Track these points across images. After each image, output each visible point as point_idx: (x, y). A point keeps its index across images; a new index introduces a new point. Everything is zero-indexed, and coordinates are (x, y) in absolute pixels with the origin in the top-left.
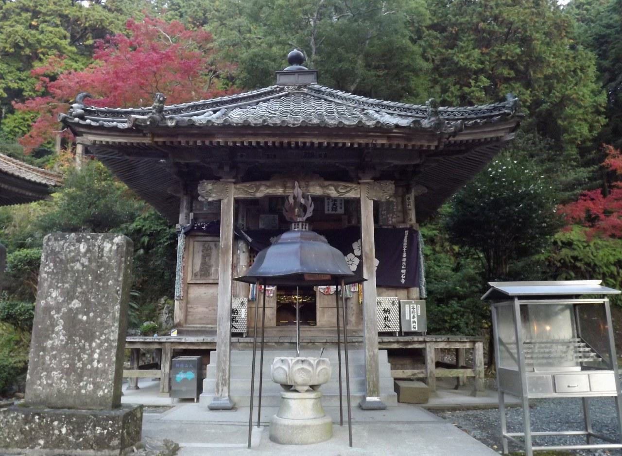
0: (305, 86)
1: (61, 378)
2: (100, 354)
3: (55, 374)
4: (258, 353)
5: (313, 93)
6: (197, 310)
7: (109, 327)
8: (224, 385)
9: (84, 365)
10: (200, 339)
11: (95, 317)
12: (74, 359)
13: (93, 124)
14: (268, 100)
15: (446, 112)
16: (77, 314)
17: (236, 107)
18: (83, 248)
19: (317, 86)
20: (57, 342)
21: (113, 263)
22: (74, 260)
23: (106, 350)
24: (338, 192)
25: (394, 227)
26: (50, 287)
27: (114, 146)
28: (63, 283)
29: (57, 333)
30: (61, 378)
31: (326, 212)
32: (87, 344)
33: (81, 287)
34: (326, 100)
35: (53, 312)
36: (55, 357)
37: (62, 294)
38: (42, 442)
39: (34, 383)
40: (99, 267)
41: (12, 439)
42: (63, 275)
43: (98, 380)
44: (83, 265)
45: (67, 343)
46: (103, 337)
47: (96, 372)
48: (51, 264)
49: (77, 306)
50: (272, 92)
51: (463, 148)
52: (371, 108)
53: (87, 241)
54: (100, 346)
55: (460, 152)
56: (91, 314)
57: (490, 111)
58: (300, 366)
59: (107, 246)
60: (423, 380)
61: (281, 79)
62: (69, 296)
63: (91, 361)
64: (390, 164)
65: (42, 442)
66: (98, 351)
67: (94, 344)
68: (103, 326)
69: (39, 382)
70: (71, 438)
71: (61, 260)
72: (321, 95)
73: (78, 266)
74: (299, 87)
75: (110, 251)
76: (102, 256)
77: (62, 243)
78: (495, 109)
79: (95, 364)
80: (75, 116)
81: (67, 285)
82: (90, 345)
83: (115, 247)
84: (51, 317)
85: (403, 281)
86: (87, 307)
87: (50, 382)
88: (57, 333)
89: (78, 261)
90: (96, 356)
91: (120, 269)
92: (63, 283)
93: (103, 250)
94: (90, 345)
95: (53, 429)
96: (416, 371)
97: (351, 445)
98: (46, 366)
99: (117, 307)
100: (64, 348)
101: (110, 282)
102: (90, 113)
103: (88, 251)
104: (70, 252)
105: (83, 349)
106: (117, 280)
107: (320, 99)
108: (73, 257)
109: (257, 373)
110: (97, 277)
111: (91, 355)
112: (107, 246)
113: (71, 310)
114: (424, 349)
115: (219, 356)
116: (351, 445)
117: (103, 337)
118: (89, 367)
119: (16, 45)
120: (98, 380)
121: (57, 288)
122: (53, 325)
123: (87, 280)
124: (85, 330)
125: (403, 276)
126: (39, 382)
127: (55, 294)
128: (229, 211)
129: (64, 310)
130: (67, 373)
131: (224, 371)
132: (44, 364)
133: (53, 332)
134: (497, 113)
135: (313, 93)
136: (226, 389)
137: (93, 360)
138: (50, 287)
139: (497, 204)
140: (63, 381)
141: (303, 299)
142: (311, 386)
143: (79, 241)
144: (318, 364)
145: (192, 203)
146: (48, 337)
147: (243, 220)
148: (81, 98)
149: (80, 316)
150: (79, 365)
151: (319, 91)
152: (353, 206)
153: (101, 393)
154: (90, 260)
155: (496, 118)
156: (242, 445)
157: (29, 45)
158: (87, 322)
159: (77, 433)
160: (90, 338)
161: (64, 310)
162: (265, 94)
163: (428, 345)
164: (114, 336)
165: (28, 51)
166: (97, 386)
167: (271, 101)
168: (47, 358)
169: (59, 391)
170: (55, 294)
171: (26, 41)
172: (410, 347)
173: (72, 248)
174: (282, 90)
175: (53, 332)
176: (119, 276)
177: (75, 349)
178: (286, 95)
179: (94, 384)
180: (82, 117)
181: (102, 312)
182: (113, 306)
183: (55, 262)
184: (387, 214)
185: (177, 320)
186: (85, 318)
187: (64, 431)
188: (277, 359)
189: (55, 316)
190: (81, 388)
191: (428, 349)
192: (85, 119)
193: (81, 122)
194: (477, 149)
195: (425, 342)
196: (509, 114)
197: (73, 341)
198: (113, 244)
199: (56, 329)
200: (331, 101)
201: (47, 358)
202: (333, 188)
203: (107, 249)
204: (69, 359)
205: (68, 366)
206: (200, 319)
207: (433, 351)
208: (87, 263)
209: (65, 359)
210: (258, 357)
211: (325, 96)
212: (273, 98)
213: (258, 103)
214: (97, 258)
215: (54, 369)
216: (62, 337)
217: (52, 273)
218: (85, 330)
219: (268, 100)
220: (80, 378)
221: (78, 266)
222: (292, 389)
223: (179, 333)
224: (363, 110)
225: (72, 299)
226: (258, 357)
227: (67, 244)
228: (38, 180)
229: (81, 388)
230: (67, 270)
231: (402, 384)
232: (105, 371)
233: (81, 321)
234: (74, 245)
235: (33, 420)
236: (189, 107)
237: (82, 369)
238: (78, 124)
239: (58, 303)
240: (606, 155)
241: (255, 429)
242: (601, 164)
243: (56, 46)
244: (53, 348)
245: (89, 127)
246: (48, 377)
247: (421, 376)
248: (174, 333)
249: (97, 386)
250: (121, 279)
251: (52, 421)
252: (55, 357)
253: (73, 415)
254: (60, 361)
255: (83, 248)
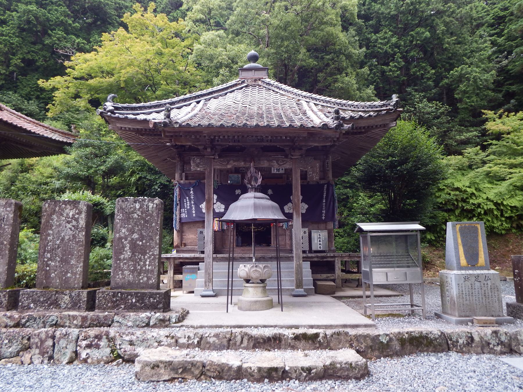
0: (260, 80)
1: (130, 275)
2: (150, 262)
3: (126, 272)
4: (231, 263)
5: (265, 85)
6: (188, 237)
7: (153, 248)
8: (209, 282)
9: (141, 268)
10: (192, 255)
11: (146, 242)
12: (136, 265)
13: (121, 116)
14: (234, 91)
15: (353, 105)
16: (136, 241)
17: (211, 98)
18: (137, 206)
19: (268, 80)
20: (126, 256)
21: (155, 214)
22: (133, 213)
23: (153, 260)
24: (279, 164)
25: (318, 182)
26: (121, 227)
27: (134, 130)
28: (128, 225)
29: (126, 251)
30: (130, 275)
31: (273, 172)
32: (142, 257)
33: (138, 227)
34: (273, 91)
35: (123, 240)
36: (125, 264)
37: (128, 231)
38: (123, 306)
39: (115, 277)
40: (147, 216)
41: (107, 305)
42: (128, 221)
43: (149, 275)
44: (138, 215)
45: (132, 257)
46: (151, 253)
47: (147, 271)
48: (121, 215)
49: (136, 237)
50: (236, 85)
51: (363, 130)
52: (304, 99)
53: (139, 202)
54: (149, 258)
55: (360, 133)
56: (144, 241)
57: (381, 106)
58: (255, 269)
59: (151, 205)
60: (334, 281)
61: (244, 74)
62: (132, 231)
63: (145, 265)
64: (311, 145)
65: (123, 306)
66: (148, 260)
67: (146, 257)
68: (151, 248)
69: (118, 277)
70: (138, 304)
71: (126, 212)
72: (270, 87)
73: (135, 216)
74: (255, 80)
75: (153, 207)
76: (148, 210)
77: (126, 203)
78: (384, 105)
79: (147, 267)
80: (109, 111)
81: (130, 226)
82: (144, 257)
83: (155, 206)
84: (122, 243)
85: (324, 218)
86: (142, 238)
87: (124, 276)
88: (126, 251)
89: (135, 213)
90: (147, 263)
91: (158, 217)
92: (128, 225)
93: (148, 207)
94: (144, 257)
95: (128, 300)
96: (329, 275)
97: (282, 311)
98: (121, 268)
99: (158, 237)
100: (130, 259)
101: (154, 224)
102: (117, 108)
103: (140, 207)
104: (131, 208)
105: (140, 259)
106: (157, 223)
107: (270, 89)
108: (133, 211)
109: (231, 275)
110: (146, 222)
111: (145, 263)
112: (151, 205)
113: (132, 239)
114: (334, 261)
115: (206, 265)
116: (282, 311)
117: (151, 253)
118: (144, 268)
119: (28, 22)
120: (149, 275)
121: (125, 228)
122: (124, 247)
123: (141, 223)
124: (141, 249)
125: (324, 215)
126: (118, 277)
127: (123, 231)
128: (211, 176)
129: (129, 239)
130: (132, 272)
131: (209, 274)
132: (120, 267)
133: (124, 250)
134: (384, 108)
135: (265, 85)
136: (210, 284)
137: (146, 265)
138: (121, 227)
139: (392, 166)
140: (131, 276)
141: (258, 228)
142: (261, 280)
143: (135, 202)
144: (265, 267)
145: (183, 166)
146: (121, 253)
147: (218, 178)
148: (110, 98)
149: (138, 242)
150: (139, 267)
151: (269, 84)
152: (288, 173)
153: (151, 282)
154: (142, 213)
155: (384, 112)
156: (223, 311)
157: (39, 23)
158: (142, 245)
159: (141, 302)
160: (144, 254)
161: (129, 239)
162: (231, 87)
163: (336, 259)
164: (157, 252)
165: (39, 28)
166: (149, 278)
167: (236, 92)
168: (122, 264)
169: (129, 281)
170: (123, 231)
171: (37, 18)
172: (325, 260)
173: (132, 206)
174: (243, 82)
175: (124, 250)
176: (158, 221)
177: (136, 260)
178: (246, 86)
179: (147, 277)
180: (112, 112)
181: (150, 240)
182: (155, 237)
183: (123, 213)
184: (313, 173)
185: (175, 244)
186: (141, 243)
187: (134, 301)
188: (241, 265)
189: (125, 242)
190: (140, 280)
191: (336, 261)
192: (115, 114)
193: (113, 115)
194: (373, 131)
195: (334, 257)
196: (392, 110)
197: (135, 256)
198: (154, 204)
199: (126, 249)
200: (278, 92)
201: (122, 264)
202: (275, 162)
203: (150, 207)
204: (133, 265)
205: (133, 268)
206: (191, 243)
207: (340, 263)
208: (140, 214)
209: (131, 265)
210: (231, 266)
211: (273, 88)
212: (237, 89)
213: (226, 94)
214: (145, 211)
215: (125, 270)
216: (129, 253)
217: (122, 219)
218: (141, 249)
219: (234, 91)
220: (139, 274)
221: (135, 216)
222: (251, 282)
223: (177, 252)
224: (299, 100)
225: (133, 233)
226: (231, 266)
227: (129, 204)
228: (61, 140)
229: (140, 280)
230: (130, 218)
231: (319, 283)
232: (152, 271)
233: (139, 245)
234: (133, 204)
235: (117, 296)
236: (180, 100)
237: (140, 269)
238: (110, 116)
239: (126, 235)
240: (487, 120)
241: (229, 305)
242: (483, 127)
243: (62, 23)
244: (124, 259)
245: (118, 118)
246: (122, 274)
247: (332, 278)
248: (174, 252)
249: (149, 278)
250: (159, 222)
251: (127, 296)
252: (125, 264)
253: (138, 293)
254: (129, 266)
255: (137, 206)
